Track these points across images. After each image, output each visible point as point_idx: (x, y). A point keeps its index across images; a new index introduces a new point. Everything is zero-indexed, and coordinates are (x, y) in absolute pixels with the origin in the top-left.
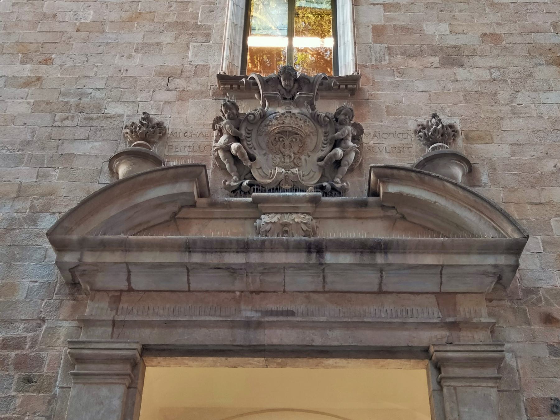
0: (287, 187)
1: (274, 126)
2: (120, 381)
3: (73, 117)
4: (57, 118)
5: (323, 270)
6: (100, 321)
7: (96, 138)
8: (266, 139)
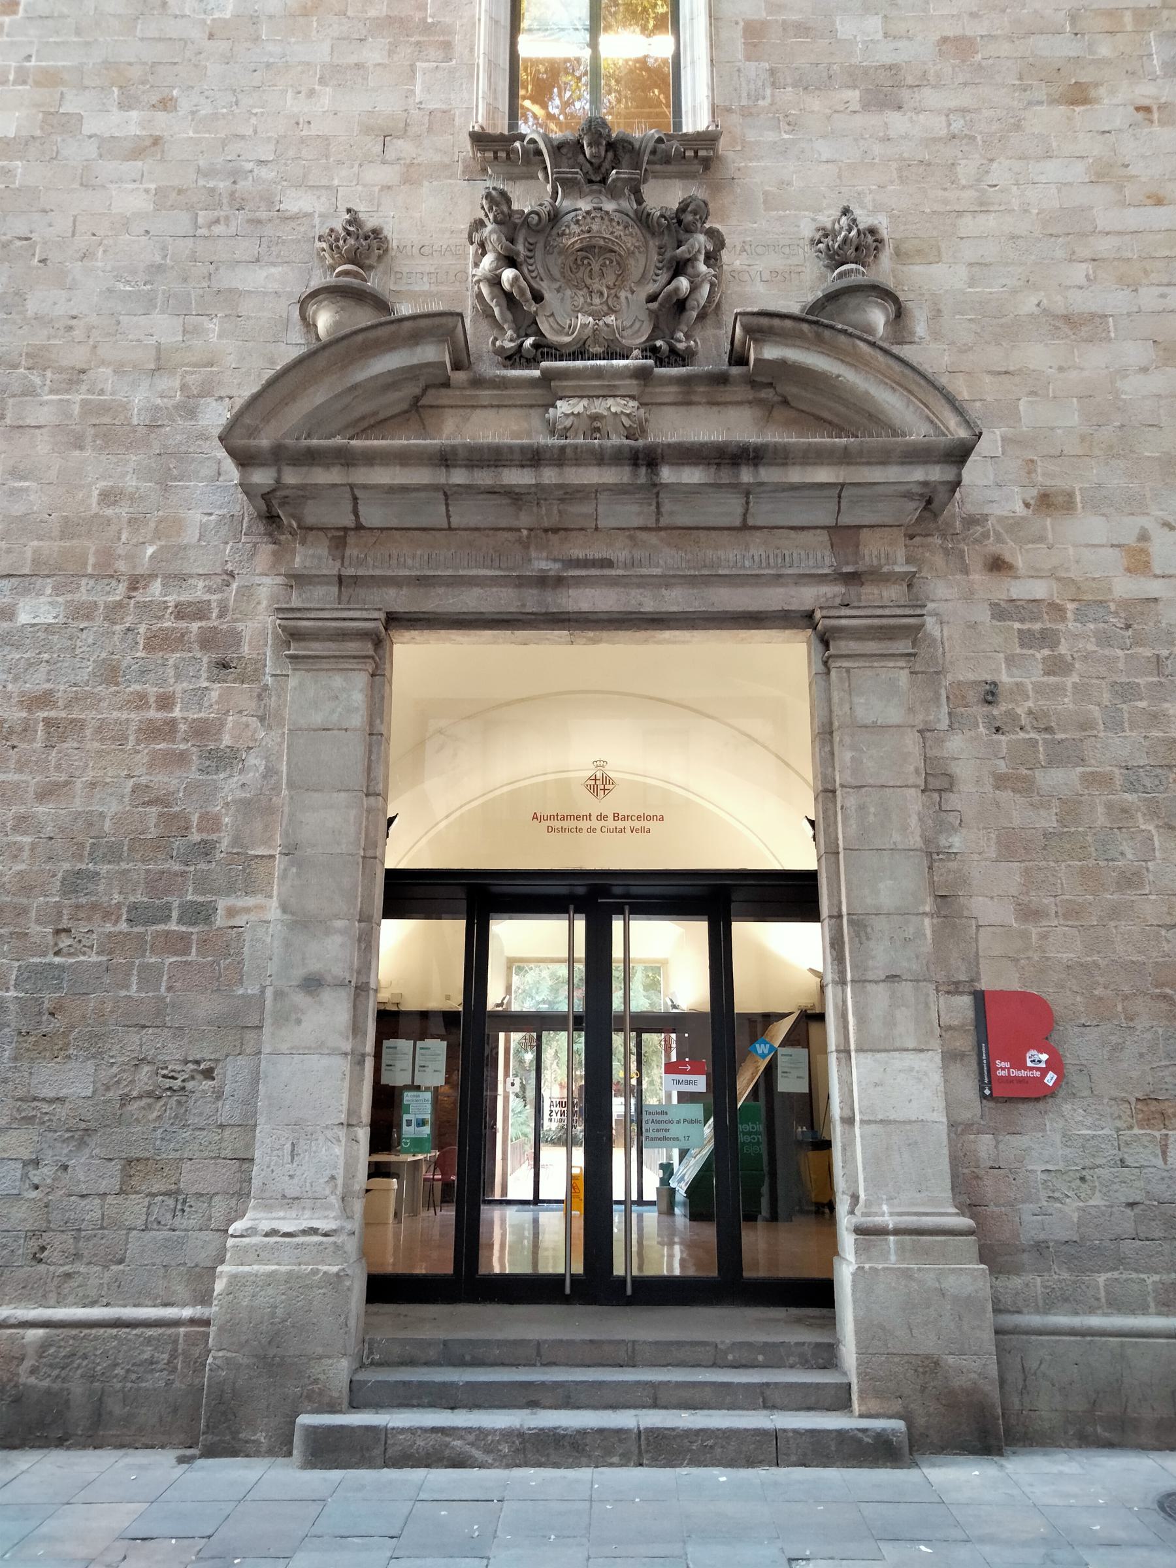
0: (598, 349)
1: (573, 237)
2: (359, 667)
3: (227, 218)
4: (200, 220)
5: (657, 494)
6: (318, 576)
7: (271, 259)
8: (560, 261)
